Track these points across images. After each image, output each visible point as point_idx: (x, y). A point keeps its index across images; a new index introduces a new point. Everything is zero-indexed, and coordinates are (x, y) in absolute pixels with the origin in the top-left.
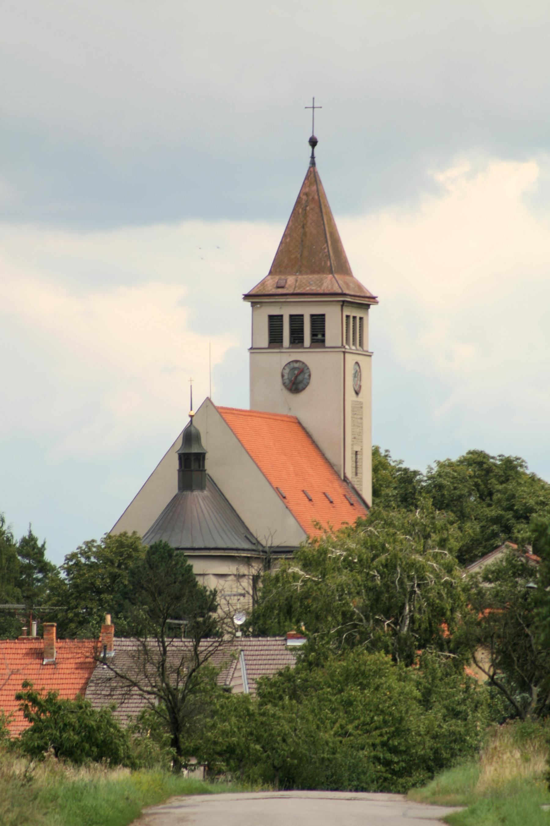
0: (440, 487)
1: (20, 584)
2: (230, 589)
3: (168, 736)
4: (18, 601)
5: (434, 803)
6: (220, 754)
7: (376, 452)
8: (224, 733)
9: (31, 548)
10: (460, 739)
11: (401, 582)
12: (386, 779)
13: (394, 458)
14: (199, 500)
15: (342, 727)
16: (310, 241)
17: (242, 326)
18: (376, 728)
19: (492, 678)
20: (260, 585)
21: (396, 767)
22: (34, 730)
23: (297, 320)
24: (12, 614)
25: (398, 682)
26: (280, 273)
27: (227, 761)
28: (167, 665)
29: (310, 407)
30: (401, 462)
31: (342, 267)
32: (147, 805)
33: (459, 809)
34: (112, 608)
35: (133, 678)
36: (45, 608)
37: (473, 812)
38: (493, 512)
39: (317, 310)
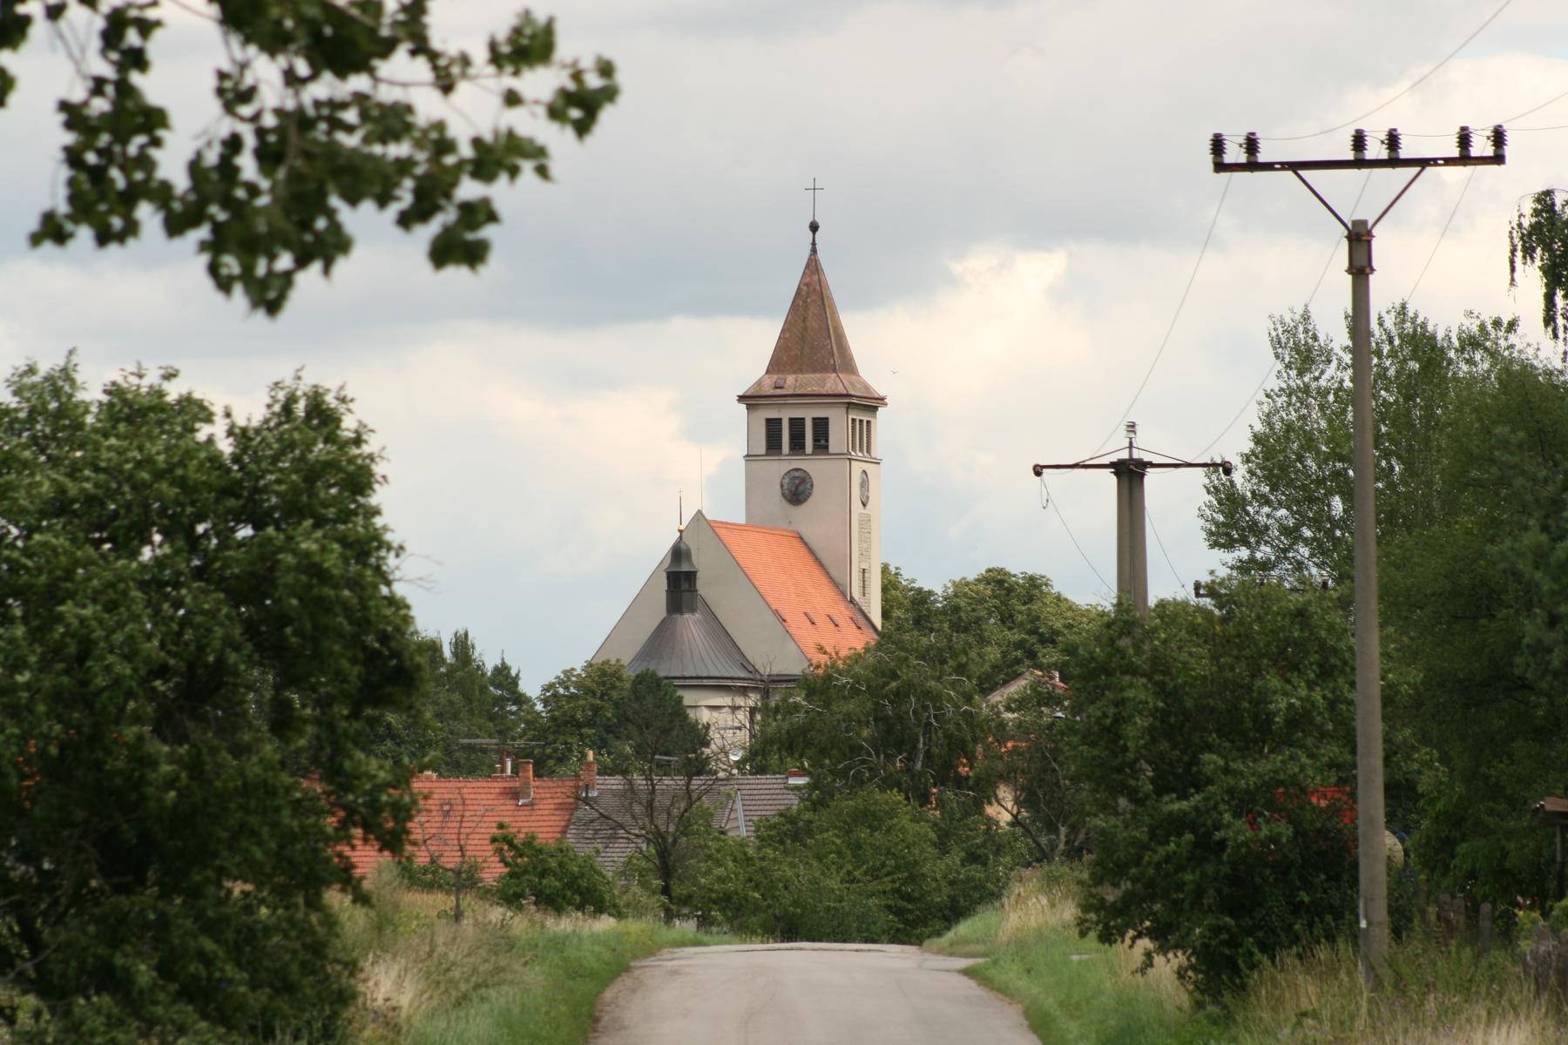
0: (956, 609)
1: (492, 718)
2: (726, 724)
3: (657, 883)
4: (490, 736)
5: (951, 954)
6: (715, 902)
7: (885, 569)
8: (721, 880)
9: (505, 677)
10: (980, 887)
11: (915, 712)
12: (898, 930)
13: (907, 575)
14: (691, 625)
15: (849, 873)
16: (811, 335)
17: (736, 433)
18: (888, 874)
19: (1015, 817)
20: (758, 717)
21: (910, 917)
22: (512, 875)
23: (797, 424)
24: (484, 751)
25: (913, 825)
26: (779, 371)
27: (723, 910)
28: (656, 804)
29: (811, 519)
30: (914, 581)
31: (848, 366)
32: (635, 958)
33: (980, 960)
34: (594, 743)
35: (619, 819)
36: (520, 743)
37: (995, 962)
38: (1016, 636)
39: (820, 413)
